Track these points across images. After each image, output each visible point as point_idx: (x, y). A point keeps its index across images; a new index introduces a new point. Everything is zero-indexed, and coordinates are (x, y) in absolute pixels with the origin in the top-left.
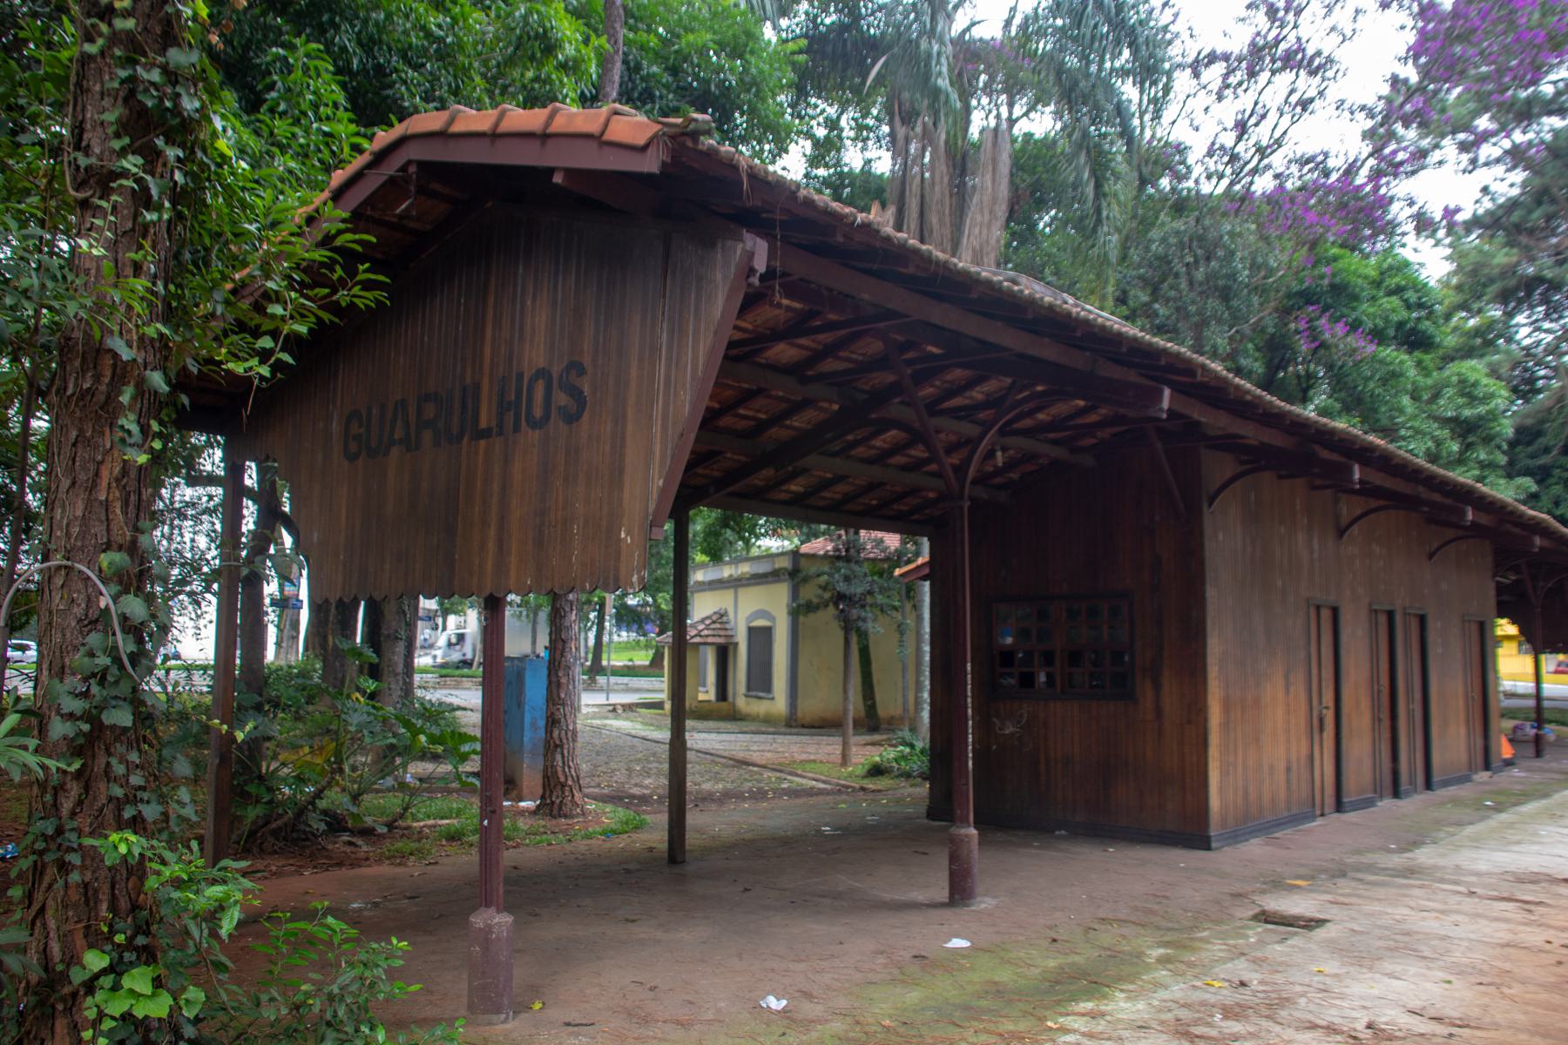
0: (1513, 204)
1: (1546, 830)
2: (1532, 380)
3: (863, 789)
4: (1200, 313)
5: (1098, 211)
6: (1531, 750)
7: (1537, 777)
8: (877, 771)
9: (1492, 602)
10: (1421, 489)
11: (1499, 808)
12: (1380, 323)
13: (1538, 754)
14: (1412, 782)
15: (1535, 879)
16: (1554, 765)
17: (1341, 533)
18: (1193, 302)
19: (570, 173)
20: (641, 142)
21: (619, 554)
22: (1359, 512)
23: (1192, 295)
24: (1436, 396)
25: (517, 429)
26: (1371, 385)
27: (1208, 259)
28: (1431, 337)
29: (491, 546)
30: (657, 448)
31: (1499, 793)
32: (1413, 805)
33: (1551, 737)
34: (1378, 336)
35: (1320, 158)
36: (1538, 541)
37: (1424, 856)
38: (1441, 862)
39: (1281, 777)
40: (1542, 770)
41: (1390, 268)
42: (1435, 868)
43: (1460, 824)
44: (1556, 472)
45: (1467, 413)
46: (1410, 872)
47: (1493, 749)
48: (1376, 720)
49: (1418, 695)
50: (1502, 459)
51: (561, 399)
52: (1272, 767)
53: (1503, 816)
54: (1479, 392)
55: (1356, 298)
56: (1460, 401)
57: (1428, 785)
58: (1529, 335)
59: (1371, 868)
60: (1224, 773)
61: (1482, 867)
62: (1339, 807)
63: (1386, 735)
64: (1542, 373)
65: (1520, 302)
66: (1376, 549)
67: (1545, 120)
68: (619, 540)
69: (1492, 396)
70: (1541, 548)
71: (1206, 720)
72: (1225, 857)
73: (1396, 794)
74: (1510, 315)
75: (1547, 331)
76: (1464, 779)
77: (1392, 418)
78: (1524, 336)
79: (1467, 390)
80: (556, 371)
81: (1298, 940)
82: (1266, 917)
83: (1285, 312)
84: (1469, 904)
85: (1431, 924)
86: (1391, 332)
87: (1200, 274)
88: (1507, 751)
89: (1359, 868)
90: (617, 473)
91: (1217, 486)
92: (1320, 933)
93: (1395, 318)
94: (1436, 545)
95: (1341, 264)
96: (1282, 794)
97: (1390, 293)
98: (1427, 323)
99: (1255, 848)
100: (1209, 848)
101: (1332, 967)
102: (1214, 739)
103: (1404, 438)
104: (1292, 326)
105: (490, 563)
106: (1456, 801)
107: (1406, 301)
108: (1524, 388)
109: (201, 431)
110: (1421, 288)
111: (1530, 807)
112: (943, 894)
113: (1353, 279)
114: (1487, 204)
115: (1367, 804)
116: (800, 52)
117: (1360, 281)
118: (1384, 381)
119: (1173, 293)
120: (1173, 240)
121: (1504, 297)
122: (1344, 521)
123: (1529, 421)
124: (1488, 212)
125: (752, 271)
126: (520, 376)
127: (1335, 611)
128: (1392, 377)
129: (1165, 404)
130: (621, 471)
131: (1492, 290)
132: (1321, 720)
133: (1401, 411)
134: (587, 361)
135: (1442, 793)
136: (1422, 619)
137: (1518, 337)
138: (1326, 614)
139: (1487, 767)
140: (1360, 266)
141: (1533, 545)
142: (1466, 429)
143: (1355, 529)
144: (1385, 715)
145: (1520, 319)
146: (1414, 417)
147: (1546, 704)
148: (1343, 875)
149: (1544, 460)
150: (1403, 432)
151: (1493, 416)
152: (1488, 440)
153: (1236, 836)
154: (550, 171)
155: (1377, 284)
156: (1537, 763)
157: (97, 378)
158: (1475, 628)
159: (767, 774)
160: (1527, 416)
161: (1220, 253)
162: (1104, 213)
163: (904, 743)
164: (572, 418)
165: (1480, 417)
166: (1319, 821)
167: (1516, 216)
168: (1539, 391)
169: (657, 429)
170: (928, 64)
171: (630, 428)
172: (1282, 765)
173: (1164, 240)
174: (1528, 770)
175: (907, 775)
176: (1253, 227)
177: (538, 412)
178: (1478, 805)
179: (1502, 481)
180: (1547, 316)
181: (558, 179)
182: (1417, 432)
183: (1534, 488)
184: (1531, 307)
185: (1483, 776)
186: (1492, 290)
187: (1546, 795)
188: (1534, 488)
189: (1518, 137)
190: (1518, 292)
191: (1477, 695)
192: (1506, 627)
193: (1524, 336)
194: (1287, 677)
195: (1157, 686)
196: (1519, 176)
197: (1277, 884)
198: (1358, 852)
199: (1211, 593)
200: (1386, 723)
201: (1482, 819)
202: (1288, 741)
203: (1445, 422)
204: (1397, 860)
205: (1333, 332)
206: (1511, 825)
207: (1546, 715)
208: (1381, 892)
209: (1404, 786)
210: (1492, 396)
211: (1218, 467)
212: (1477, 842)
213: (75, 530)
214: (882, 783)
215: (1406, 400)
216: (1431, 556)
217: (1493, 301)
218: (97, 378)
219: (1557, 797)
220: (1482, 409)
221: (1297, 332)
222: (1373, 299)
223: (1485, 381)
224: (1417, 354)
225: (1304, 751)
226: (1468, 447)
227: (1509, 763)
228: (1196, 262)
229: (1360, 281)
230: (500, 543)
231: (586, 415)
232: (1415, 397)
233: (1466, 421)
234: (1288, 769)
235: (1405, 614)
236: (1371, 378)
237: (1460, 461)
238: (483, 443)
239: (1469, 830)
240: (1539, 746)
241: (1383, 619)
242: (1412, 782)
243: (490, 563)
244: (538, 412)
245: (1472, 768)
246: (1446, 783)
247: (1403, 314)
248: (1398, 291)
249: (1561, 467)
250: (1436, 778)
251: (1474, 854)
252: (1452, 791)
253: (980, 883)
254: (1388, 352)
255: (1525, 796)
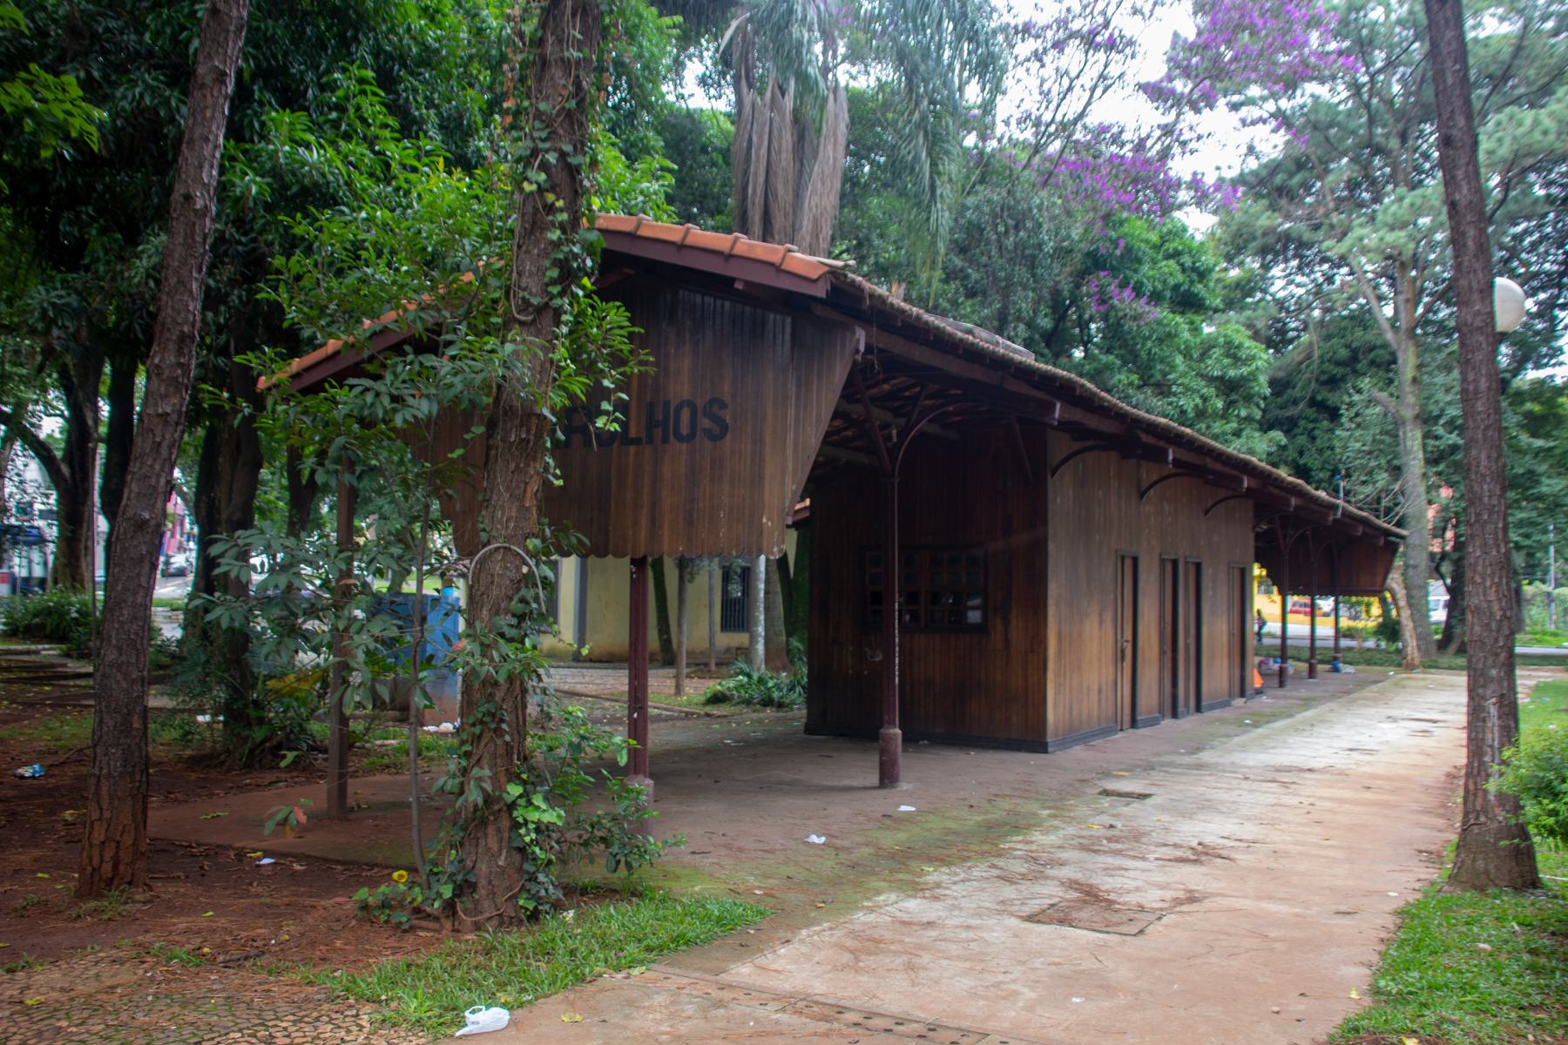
0: (1274, 168)
1: (1294, 740)
2: (1282, 331)
3: (708, 715)
4: (1009, 278)
5: (933, 188)
6: (1275, 681)
7: (1282, 703)
8: (717, 699)
9: (1252, 551)
10: (1208, 460)
11: (1256, 725)
12: (1159, 286)
13: (1281, 684)
14: (1187, 705)
15: (1289, 769)
16: (1295, 694)
17: (1142, 495)
18: (1002, 268)
19: (747, 283)
20: (815, 276)
21: (761, 534)
22: (1155, 477)
23: (1000, 262)
24: (1204, 355)
25: (665, 440)
26: (1149, 344)
27: (1016, 227)
28: (1203, 299)
29: (644, 521)
30: (790, 465)
31: (1254, 714)
32: (1188, 724)
33: (1291, 671)
34: (1156, 297)
35: (1115, 130)
36: (1293, 501)
37: (1206, 756)
38: (1221, 760)
39: (1094, 697)
40: (1284, 697)
41: (1170, 232)
42: (1218, 764)
43: (1227, 736)
44: (1302, 423)
45: (1232, 373)
46: (1200, 766)
47: (1248, 679)
48: (1162, 652)
49: (1193, 631)
50: (1258, 415)
51: (706, 423)
52: (1089, 690)
53: (1260, 731)
54: (1243, 354)
55: (1139, 261)
56: (1226, 361)
57: (1198, 709)
58: (1283, 288)
59: (1171, 764)
60: (1057, 693)
61: (1251, 763)
62: (1134, 723)
63: (1168, 665)
64: (1293, 325)
65: (1276, 254)
66: (1167, 507)
67: (1306, 85)
68: (761, 524)
69: (1253, 358)
70: (1296, 507)
71: (1045, 650)
72: (1067, 760)
73: (1175, 715)
74: (1266, 267)
75: (1298, 285)
76: (1225, 704)
77: (1165, 374)
78: (1278, 288)
79: (1232, 352)
80: (700, 403)
81: (1137, 805)
82: (1106, 793)
83: (1081, 276)
84: (1245, 784)
85: (1223, 795)
86: (1168, 294)
87: (1010, 241)
88: (1257, 682)
89: (1162, 764)
90: (757, 480)
91: (1064, 455)
92: (1148, 801)
93: (1171, 281)
94: (1210, 503)
95: (1126, 229)
96: (1095, 713)
97: (1168, 257)
98: (1200, 286)
99: (1078, 751)
100: (1046, 752)
101: (1165, 818)
102: (1051, 665)
103: (1175, 394)
104: (1084, 289)
105: (643, 533)
106: (1222, 721)
107: (1182, 265)
108: (1277, 339)
109: (112, 371)
110: (1195, 252)
111: (1279, 724)
112: (874, 779)
113: (1137, 244)
114: (1253, 164)
115: (1153, 722)
116: (675, 26)
117: (1143, 245)
118: (1160, 341)
119: (984, 259)
120: (986, 209)
121: (1263, 251)
122: (1144, 485)
123: (1281, 374)
124: (1252, 172)
125: (857, 351)
126: (667, 404)
127: (1135, 560)
128: (1170, 336)
129: (1057, 415)
130: (761, 478)
131: (1253, 245)
132: (1123, 651)
133: (1173, 368)
134: (727, 399)
135: (1208, 715)
136: (1198, 567)
137: (1272, 289)
138: (1128, 563)
139: (1242, 694)
140: (1139, 230)
141: (1289, 504)
142: (1231, 388)
143: (1152, 492)
144: (1168, 648)
145: (1276, 271)
146: (1184, 375)
147: (1289, 642)
148: (1153, 769)
149: (1292, 411)
150: (1174, 388)
151: (1252, 377)
152: (1248, 399)
153: (1065, 744)
154: (733, 280)
155: (1156, 248)
156: (1281, 692)
157: (528, 431)
158: (1237, 574)
159: (607, 704)
160: (1280, 369)
161: (1029, 224)
162: (938, 192)
163: (742, 673)
164: (716, 437)
165: (1242, 377)
166: (1120, 735)
167: (1279, 179)
168: (1291, 341)
169: (789, 452)
170: (799, 53)
171: (768, 450)
172: (1096, 688)
173: (977, 208)
174: (1274, 697)
175: (748, 702)
176: (1059, 202)
177: (685, 430)
178: (1240, 724)
179: (1257, 434)
180: (1300, 268)
181: (739, 286)
182: (1187, 389)
183: (1284, 441)
184: (1286, 261)
185: (1239, 702)
186: (1253, 245)
187: (1290, 716)
188: (1284, 441)
189: (1284, 104)
190: (1275, 247)
191: (1236, 630)
192: (1257, 571)
193: (1278, 288)
194: (1100, 616)
195: (1006, 621)
196: (1282, 137)
197: (1107, 774)
198: (1157, 754)
199: (1051, 547)
200: (1169, 655)
201: (1245, 732)
202: (1100, 668)
203: (1211, 380)
204: (1187, 760)
205: (1124, 301)
206: (1266, 737)
207: (1290, 652)
208: (1183, 779)
209: (1181, 708)
210: (1253, 358)
211: (1060, 446)
212: (1243, 748)
213: (512, 525)
214: (723, 710)
215: (1179, 359)
216: (1207, 512)
217: (1255, 254)
218: (528, 431)
219: (1299, 717)
220: (1245, 370)
221: (1089, 295)
222: (1154, 262)
223: (1248, 343)
224: (1190, 316)
225: (1111, 677)
226: (1230, 404)
227: (1259, 692)
228: (1007, 232)
229: (1143, 245)
230: (653, 520)
231: (728, 437)
232: (1187, 355)
233: (1231, 380)
234: (1100, 691)
235: (1186, 563)
236: (1149, 337)
237: (1224, 416)
238: (632, 449)
239: (1236, 740)
240: (1282, 677)
241: (1169, 567)
242: (1187, 705)
243: (643, 533)
244: (685, 430)
245: (1231, 696)
246: (1212, 707)
247: (1180, 278)
248: (1176, 255)
249: (1306, 418)
250: (1204, 703)
251: (1243, 755)
252: (1216, 713)
253: (903, 773)
254: (1162, 313)
255: (1274, 717)
